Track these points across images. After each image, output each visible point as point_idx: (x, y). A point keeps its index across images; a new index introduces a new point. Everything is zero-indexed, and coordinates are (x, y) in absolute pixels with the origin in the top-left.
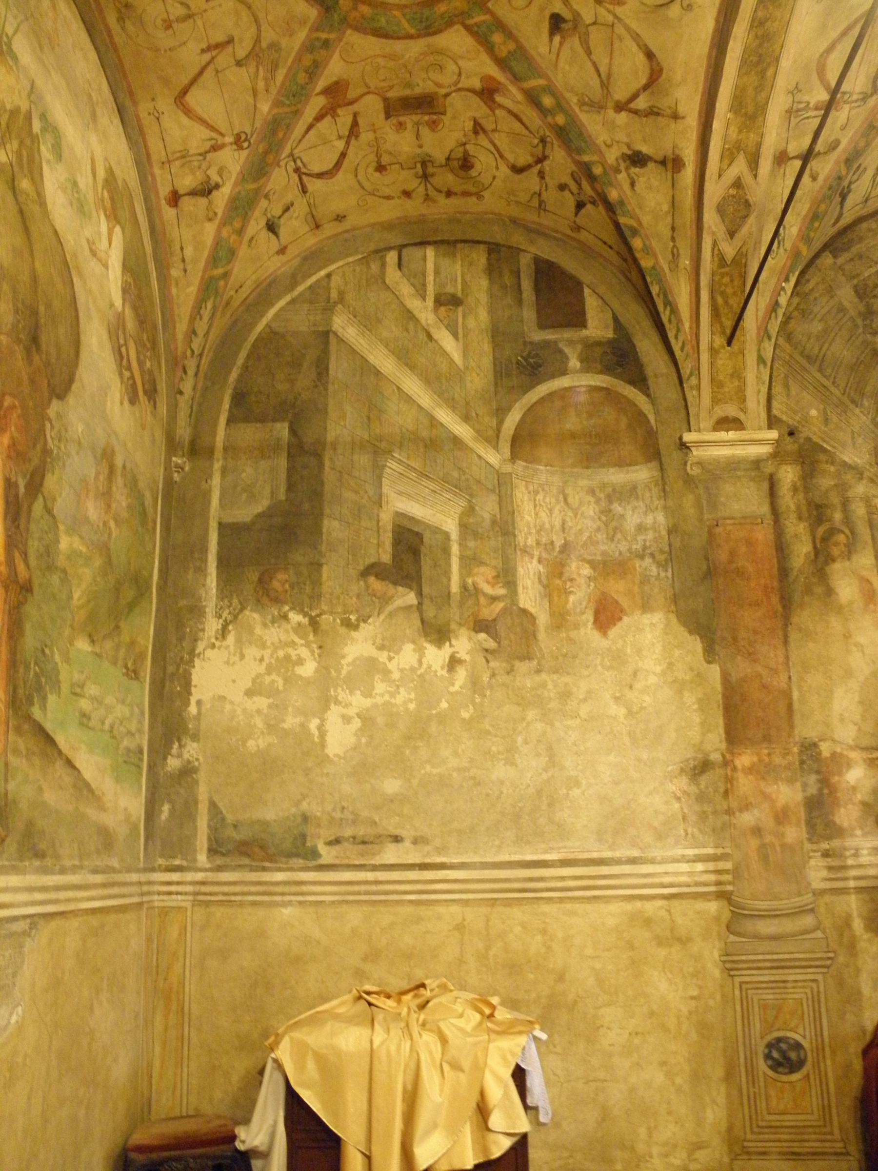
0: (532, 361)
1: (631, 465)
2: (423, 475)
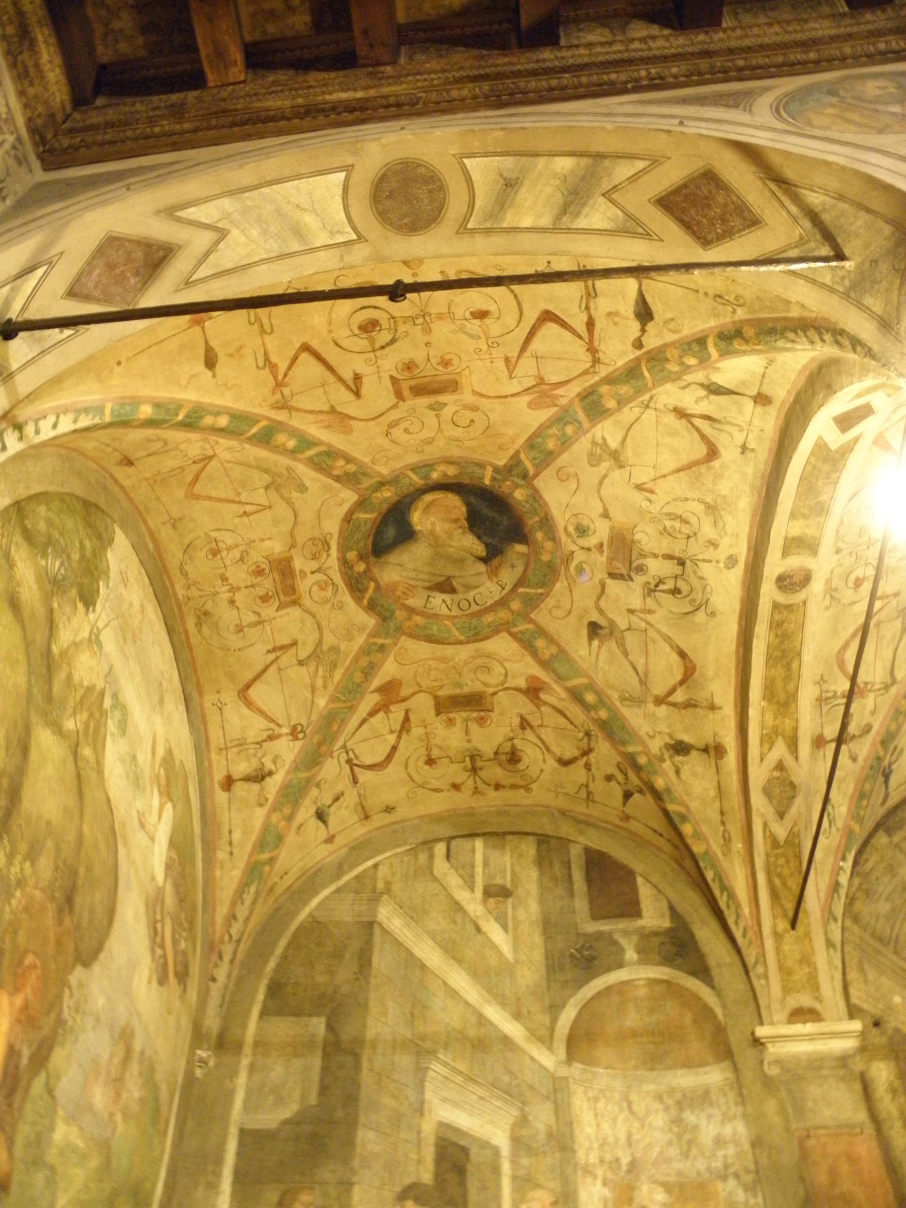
0: (586, 953)
2: (470, 1079)
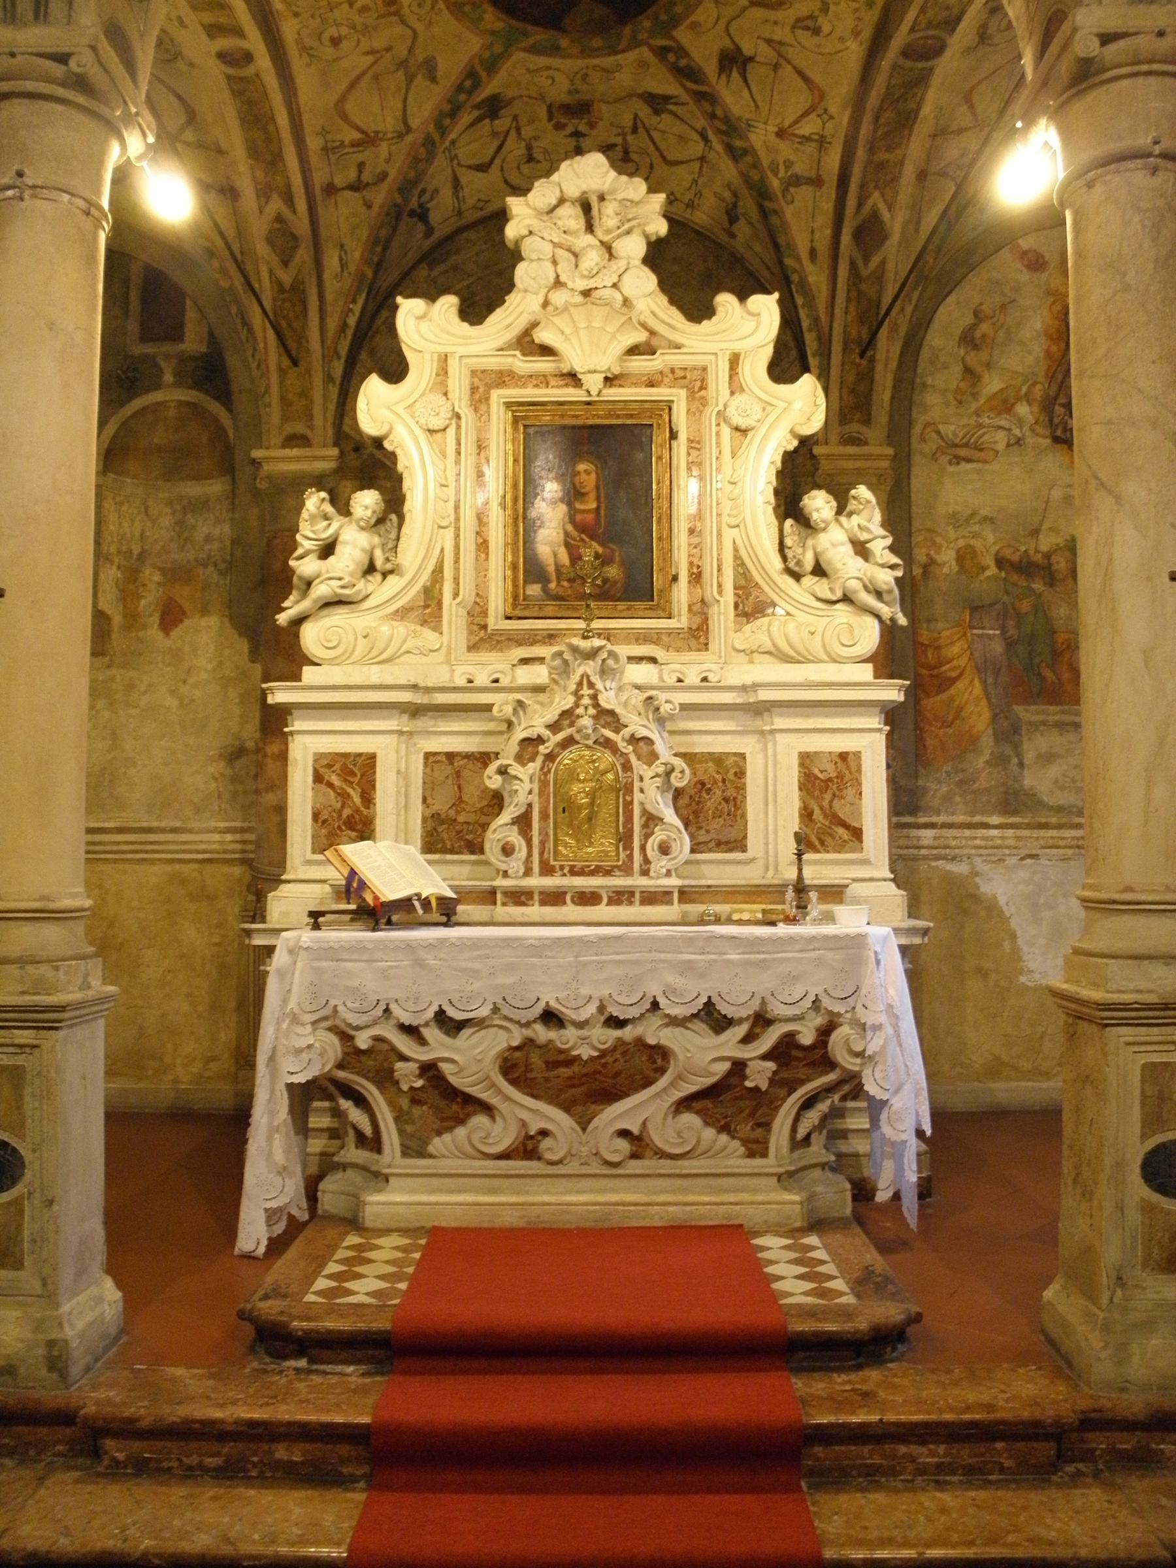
1: (206, 479)
